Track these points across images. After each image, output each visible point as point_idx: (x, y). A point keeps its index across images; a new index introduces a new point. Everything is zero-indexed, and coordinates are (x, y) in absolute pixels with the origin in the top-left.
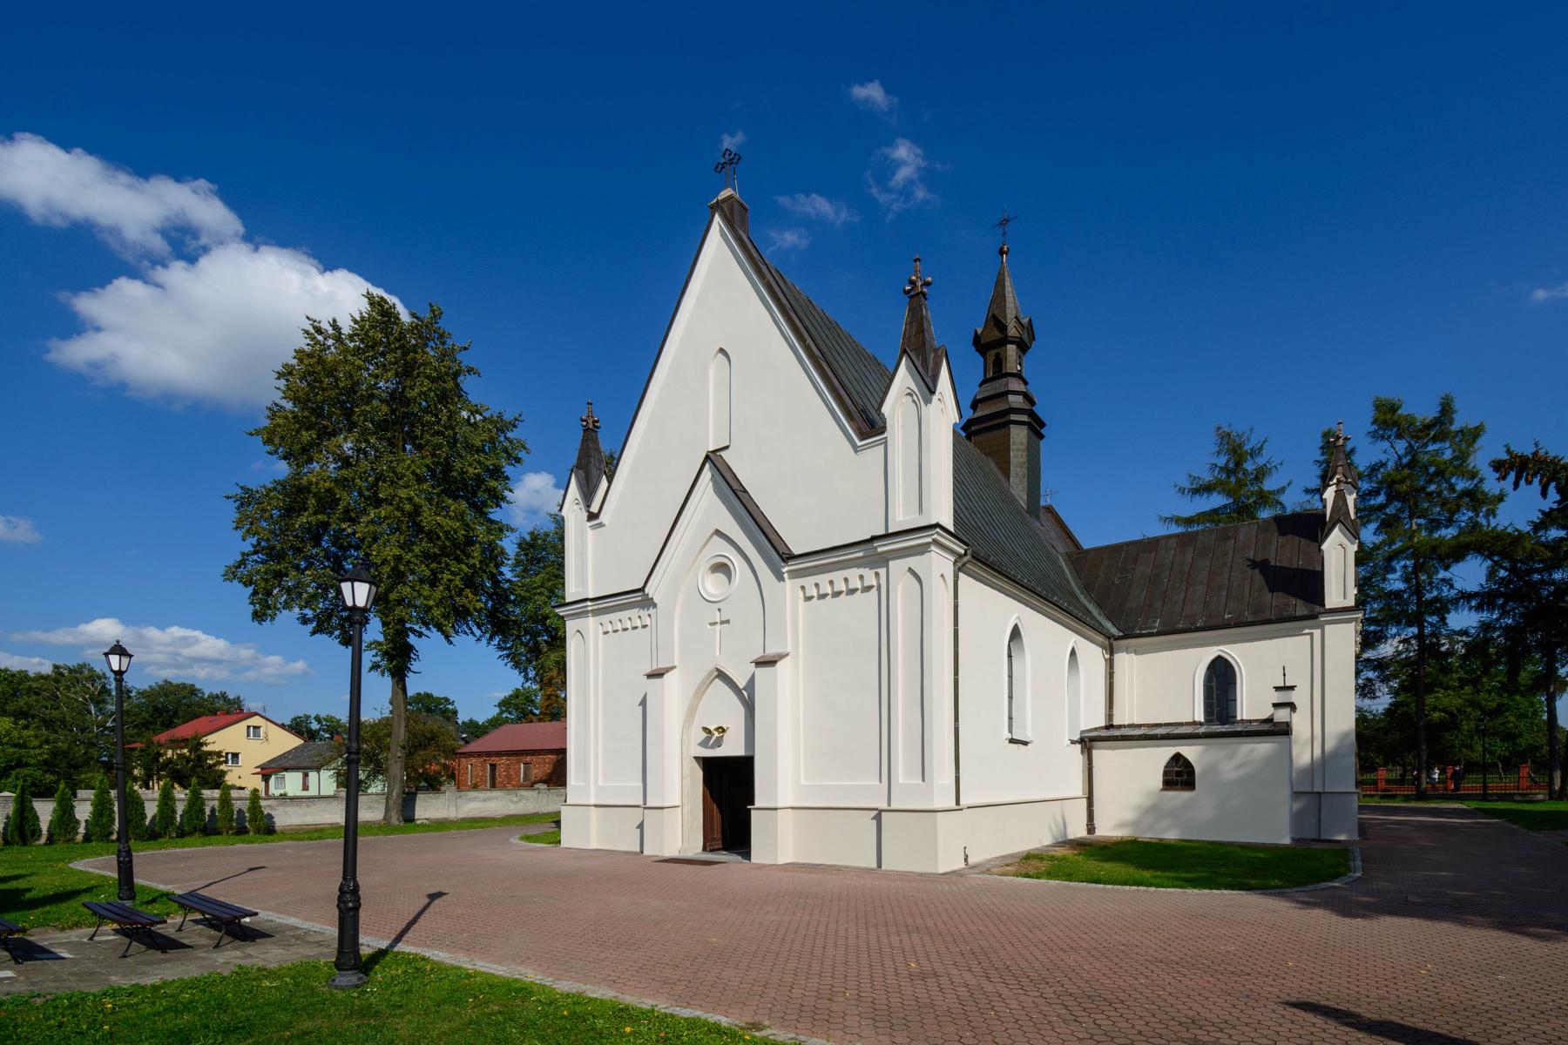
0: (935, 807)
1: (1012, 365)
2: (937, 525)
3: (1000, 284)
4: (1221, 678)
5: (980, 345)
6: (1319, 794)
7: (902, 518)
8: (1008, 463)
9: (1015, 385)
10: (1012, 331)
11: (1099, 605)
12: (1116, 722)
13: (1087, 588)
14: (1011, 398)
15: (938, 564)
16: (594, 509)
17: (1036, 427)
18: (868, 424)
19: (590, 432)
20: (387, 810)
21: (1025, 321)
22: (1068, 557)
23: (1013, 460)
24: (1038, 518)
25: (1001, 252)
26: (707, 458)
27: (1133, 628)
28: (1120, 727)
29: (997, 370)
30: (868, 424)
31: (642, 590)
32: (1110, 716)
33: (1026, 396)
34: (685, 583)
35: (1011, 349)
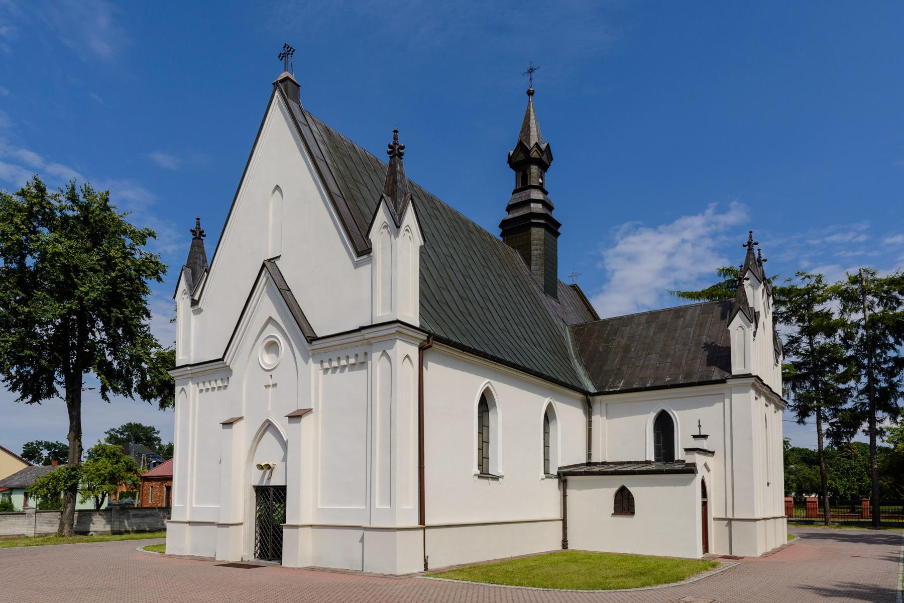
0: (756, 517)
1: (535, 180)
2: (398, 321)
3: (528, 117)
4: (664, 427)
5: (513, 162)
6: (730, 520)
7: (381, 315)
8: (530, 254)
9: (536, 195)
10: (534, 155)
11: (587, 367)
12: (593, 460)
13: (580, 354)
14: (532, 205)
15: (405, 350)
16: (196, 298)
17: (552, 227)
18: (362, 249)
19: (198, 235)
20: (62, 525)
21: (543, 146)
22: (578, 331)
23: (534, 252)
24: (554, 296)
25: (530, 93)
26: (264, 265)
27: (604, 387)
28: (596, 464)
29: (524, 184)
30: (362, 249)
31: (222, 359)
32: (589, 456)
33: (545, 204)
34: (250, 360)
35: (534, 169)
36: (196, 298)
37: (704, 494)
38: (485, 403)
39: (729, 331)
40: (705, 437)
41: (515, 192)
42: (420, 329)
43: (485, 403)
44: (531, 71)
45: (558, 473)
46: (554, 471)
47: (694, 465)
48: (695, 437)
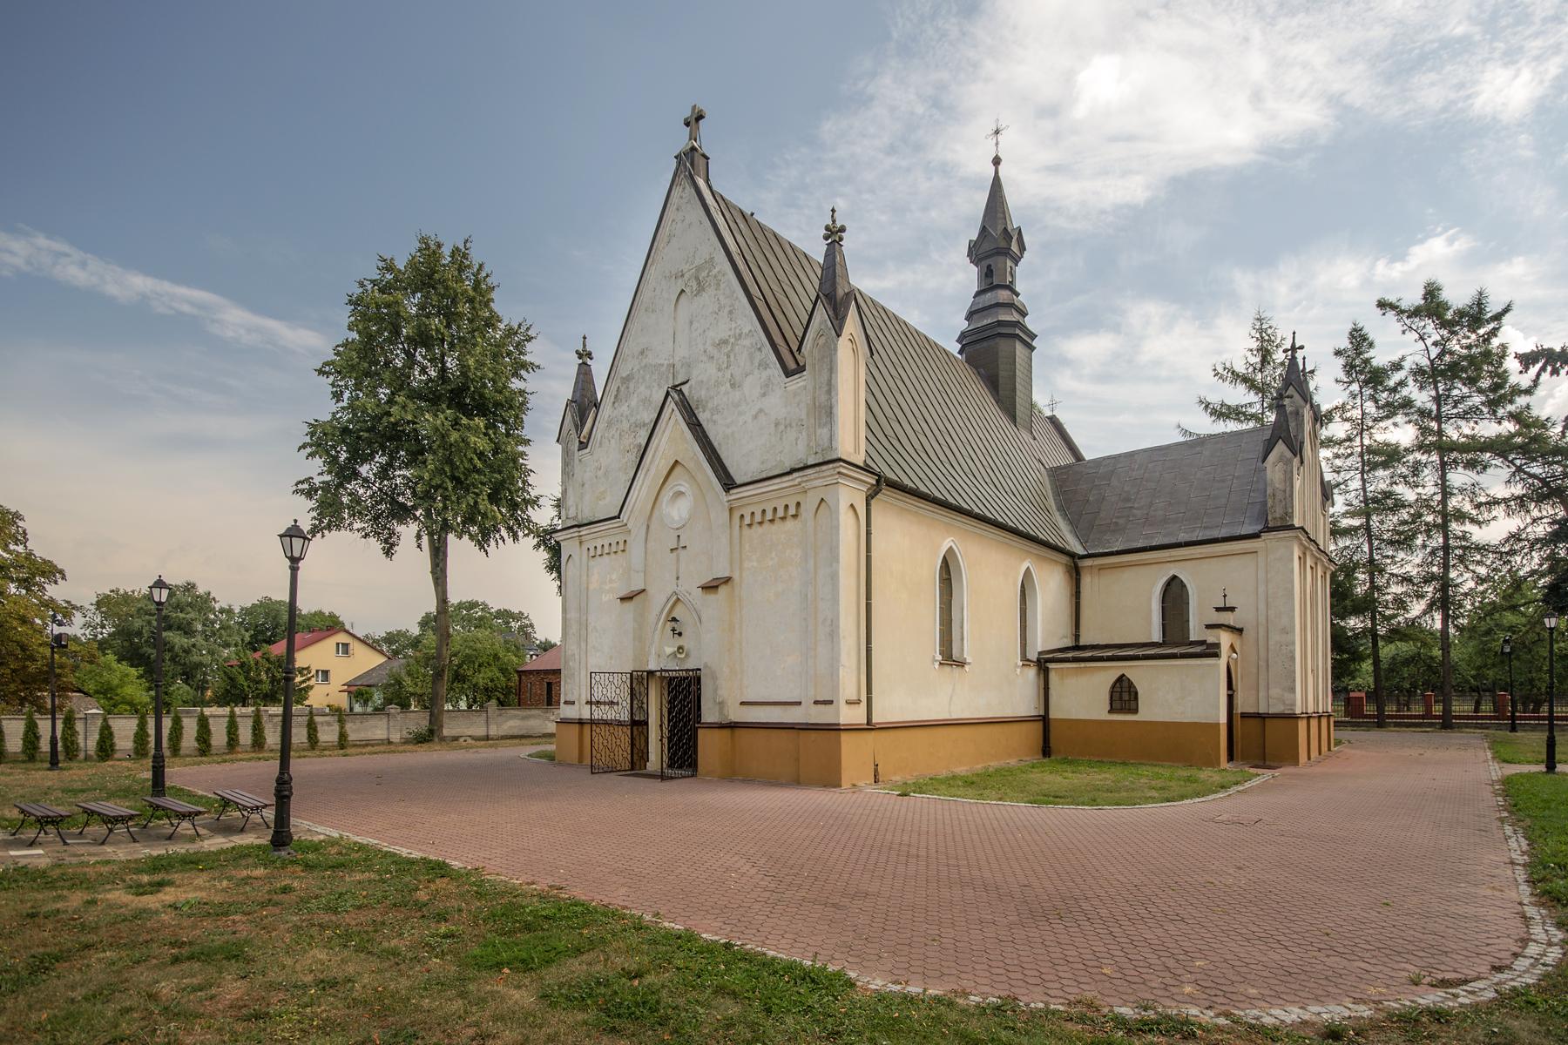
2: (840, 460)
4: (1174, 595)
28: (1085, 648)
32: (1077, 637)
36: (296, 554)
37: (1230, 686)
38: (948, 571)
39: (197, 740)
40: (1232, 609)
41: (978, 294)
42: (866, 469)
43: (948, 571)
44: (997, 132)
45: (1039, 660)
46: (1033, 656)
47: (1217, 645)
48: (1218, 609)
